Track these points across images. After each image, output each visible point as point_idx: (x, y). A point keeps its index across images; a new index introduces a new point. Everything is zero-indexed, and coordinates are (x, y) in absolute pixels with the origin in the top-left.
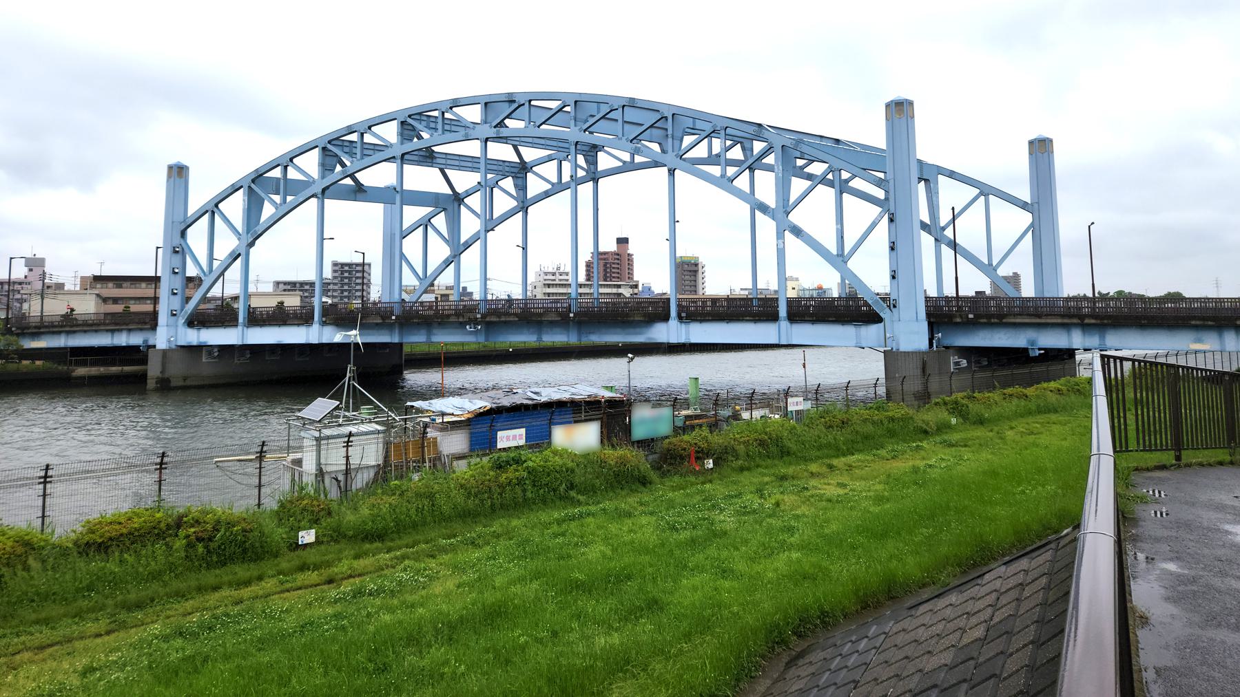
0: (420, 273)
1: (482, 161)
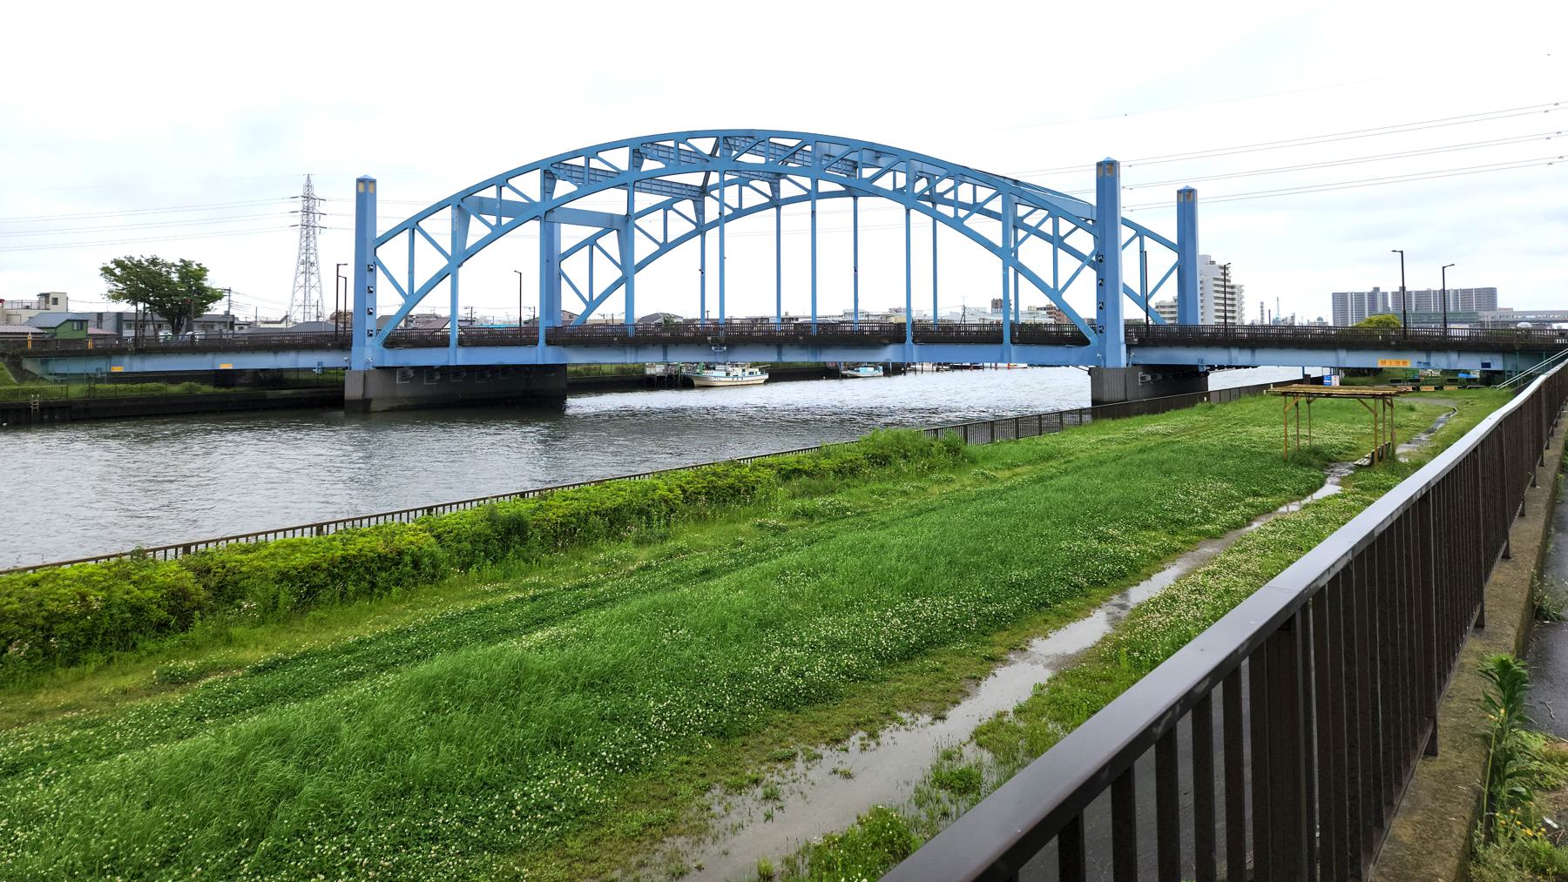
0: (406, 290)
1: (586, 169)
